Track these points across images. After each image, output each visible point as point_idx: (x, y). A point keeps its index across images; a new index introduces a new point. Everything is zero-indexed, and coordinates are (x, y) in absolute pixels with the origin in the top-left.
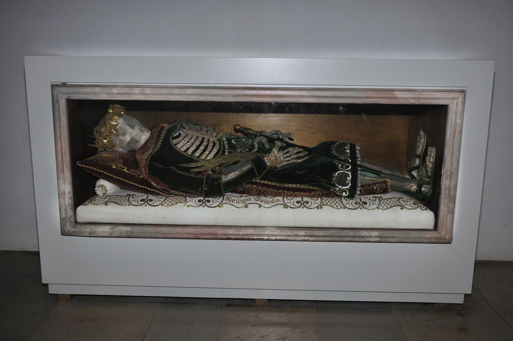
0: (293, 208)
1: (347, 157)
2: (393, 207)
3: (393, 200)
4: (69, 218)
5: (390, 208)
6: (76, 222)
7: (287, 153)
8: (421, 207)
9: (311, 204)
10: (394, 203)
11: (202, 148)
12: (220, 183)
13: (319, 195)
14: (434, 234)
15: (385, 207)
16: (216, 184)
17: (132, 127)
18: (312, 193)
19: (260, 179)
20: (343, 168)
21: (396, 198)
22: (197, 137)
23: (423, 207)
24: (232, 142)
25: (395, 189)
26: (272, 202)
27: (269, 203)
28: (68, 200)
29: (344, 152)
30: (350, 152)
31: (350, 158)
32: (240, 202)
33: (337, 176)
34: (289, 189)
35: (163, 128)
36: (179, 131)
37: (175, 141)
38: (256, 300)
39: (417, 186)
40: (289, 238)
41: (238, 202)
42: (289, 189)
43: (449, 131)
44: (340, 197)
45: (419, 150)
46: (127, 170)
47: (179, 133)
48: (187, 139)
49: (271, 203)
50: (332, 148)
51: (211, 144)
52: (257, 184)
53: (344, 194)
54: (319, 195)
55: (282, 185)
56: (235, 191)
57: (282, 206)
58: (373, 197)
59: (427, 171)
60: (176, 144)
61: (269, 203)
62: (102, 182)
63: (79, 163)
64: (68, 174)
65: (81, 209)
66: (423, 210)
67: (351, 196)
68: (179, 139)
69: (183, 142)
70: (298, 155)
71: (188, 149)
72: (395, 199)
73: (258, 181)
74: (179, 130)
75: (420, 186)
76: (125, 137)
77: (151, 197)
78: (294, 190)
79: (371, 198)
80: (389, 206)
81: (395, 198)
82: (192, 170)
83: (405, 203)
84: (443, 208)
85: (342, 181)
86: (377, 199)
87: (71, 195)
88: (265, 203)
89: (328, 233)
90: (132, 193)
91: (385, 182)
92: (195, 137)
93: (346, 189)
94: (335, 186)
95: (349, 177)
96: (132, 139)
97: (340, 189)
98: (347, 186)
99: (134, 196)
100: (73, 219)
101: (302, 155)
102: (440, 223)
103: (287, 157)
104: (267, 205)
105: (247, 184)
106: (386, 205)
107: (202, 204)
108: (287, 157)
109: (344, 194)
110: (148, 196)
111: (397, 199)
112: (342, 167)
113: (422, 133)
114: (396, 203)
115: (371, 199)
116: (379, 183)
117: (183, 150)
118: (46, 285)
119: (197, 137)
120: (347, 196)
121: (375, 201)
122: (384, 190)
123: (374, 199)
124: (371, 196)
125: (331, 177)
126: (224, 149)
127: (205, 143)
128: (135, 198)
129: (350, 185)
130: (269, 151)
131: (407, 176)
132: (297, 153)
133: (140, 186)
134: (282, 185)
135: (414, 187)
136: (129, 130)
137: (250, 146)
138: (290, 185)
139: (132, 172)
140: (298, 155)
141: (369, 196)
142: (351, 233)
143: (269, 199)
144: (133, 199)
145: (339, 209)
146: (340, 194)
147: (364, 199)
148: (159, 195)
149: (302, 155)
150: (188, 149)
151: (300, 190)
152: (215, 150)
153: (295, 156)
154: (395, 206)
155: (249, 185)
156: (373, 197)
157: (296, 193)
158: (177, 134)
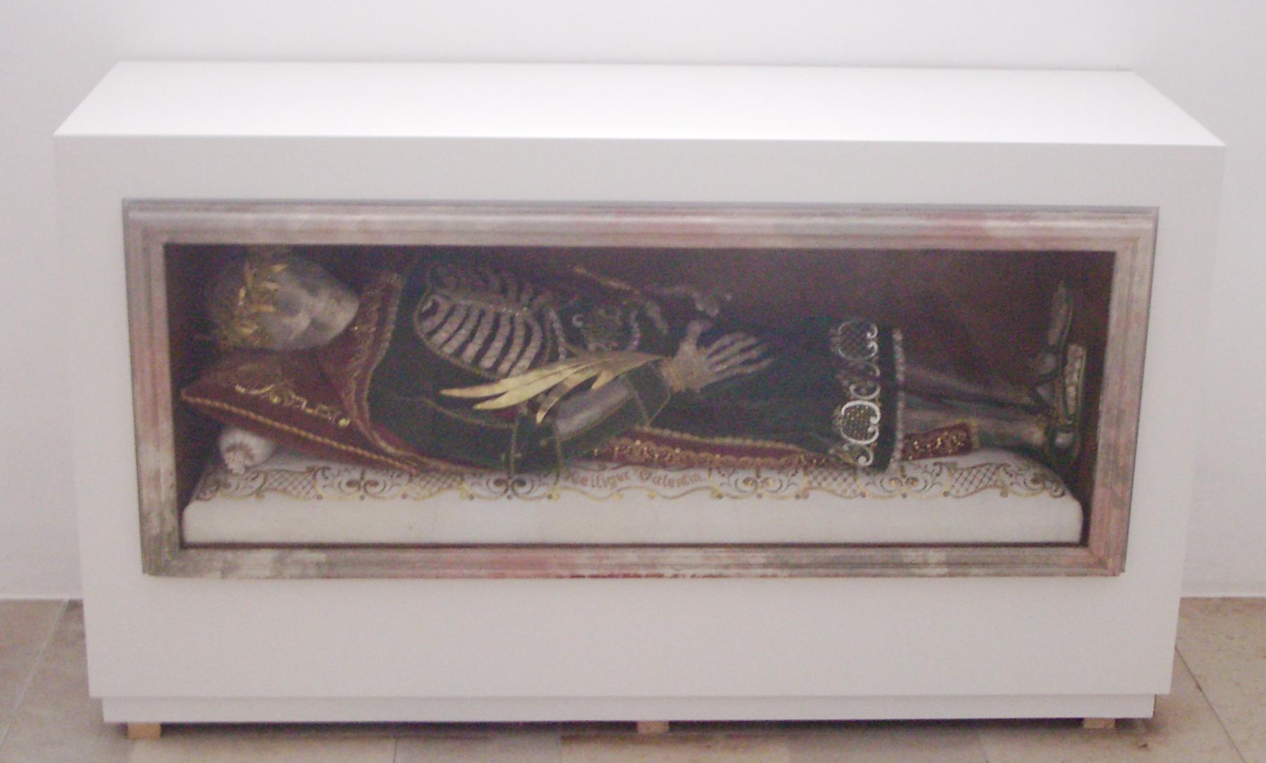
0: (735, 497)
1: (870, 360)
2: (981, 489)
3: (983, 470)
4: (169, 535)
5: (975, 492)
6: (184, 545)
7: (717, 352)
8: (1051, 488)
9: (780, 488)
10: (985, 480)
11: (498, 345)
12: (552, 444)
13: (800, 462)
14: (1080, 553)
15: (962, 492)
16: (543, 443)
17: (313, 291)
18: (783, 460)
19: (652, 425)
20: (861, 394)
21: (990, 464)
22: (482, 314)
23: (1054, 488)
24: (574, 319)
25: (988, 444)
26: (683, 482)
27: (676, 484)
28: (166, 490)
29: (865, 348)
30: (880, 348)
31: (879, 363)
32: (601, 483)
33: (846, 414)
34: (722, 450)
35: (389, 290)
36: (432, 297)
37: (428, 325)
38: (640, 726)
39: (1046, 433)
40: (725, 572)
41: (595, 483)
42: (722, 450)
43: (1115, 314)
44: (852, 469)
45: (1054, 336)
46: (309, 406)
47: (433, 300)
48: (455, 321)
49: (678, 486)
50: (833, 336)
51: (520, 333)
52: (645, 437)
53: (862, 460)
54: (800, 462)
55: (707, 441)
56: (589, 457)
57: (708, 493)
58: (935, 464)
59: (1065, 403)
60: (441, 346)
61: (676, 484)
62: (237, 437)
63: (188, 394)
64: (166, 427)
65: (195, 511)
66: (1056, 497)
67: (880, 464)
68: (437, 319)
69: (449, 328)
70: (746, 356)
71: (463, 348)
72: (988, 470)
73: (647, 429)
74: (433, 292)
75: (1051, 434)
76: (295, 320)
77: (370, 475)
78: (739, 452)
79: (930, 468)
80: (972, 489)
81: (987, 467)
82: (479, 406)
83: (1012, 480)
84: (1100, 495)
85: (858, 426)
86: (945, 469)
87: (172, 480)
88: (665, 486)
89: (822, 554)
90: (321, 464)
91: (964, 427)
92: (476, 313)
93: (868, 446)
94: (839, 439)
95: (876, 416)
96: (315, 324)
97: (851, 448)
98: (871, 437)
99: (327, 473)
100: (175, 539)
101: (754, 354)
102: (1094, 531)
103: (717, 363)
104: (669, 492)
105: (618, 437)
106: (966, 484)
107: (505, 492)
108: (717, 363)
109: (862, 460)
110: (363, 474)
111: (992, 469)
112: (857, 390)
113: (1062, 291)
114: (990, 479)
115: (931, 471)
116: (950, 429)
117: (448, 350)
118: (98, 702)
119: (482, 314)
120: (870, 466)
121: (938, 475)
122: (963, 445)
123: (937, 468)
124: (929, 462)
125: (829, 419)
126: (555, 338)
127: (504, 331)
128: (331, 478)
129: (877, 435)
130: (672, 351)
131: (1026, 400)
132: (743, 351)
133: (344, 447)
134: (707, 441)
135: (1036, 435)
136: (304, 297)
137: (619, 331)
138: (728, 441)
139: (321, 411)
140: (746, 356)
141: (923, 462)
142: (877, 554)
143: (674, 475)
144: (328, 482)
145: (850, 497)
146: (851, 461)
147: (911, 471)
148: (392, 467)
149: (754, 354)
150: (463, 348)
151: (754, 452)
152: (531, 352)
153: (740, 359)
154: (986, 487)
155: (624, 441)
156: (935, 464)
157: (743, 459)
158: (429, 304)
